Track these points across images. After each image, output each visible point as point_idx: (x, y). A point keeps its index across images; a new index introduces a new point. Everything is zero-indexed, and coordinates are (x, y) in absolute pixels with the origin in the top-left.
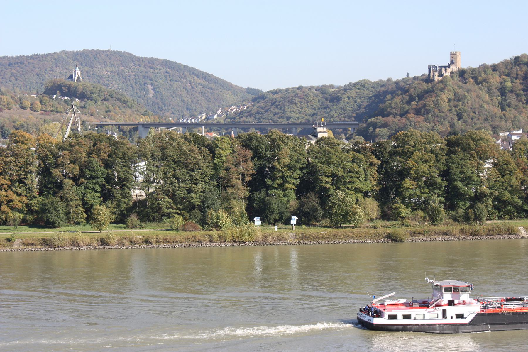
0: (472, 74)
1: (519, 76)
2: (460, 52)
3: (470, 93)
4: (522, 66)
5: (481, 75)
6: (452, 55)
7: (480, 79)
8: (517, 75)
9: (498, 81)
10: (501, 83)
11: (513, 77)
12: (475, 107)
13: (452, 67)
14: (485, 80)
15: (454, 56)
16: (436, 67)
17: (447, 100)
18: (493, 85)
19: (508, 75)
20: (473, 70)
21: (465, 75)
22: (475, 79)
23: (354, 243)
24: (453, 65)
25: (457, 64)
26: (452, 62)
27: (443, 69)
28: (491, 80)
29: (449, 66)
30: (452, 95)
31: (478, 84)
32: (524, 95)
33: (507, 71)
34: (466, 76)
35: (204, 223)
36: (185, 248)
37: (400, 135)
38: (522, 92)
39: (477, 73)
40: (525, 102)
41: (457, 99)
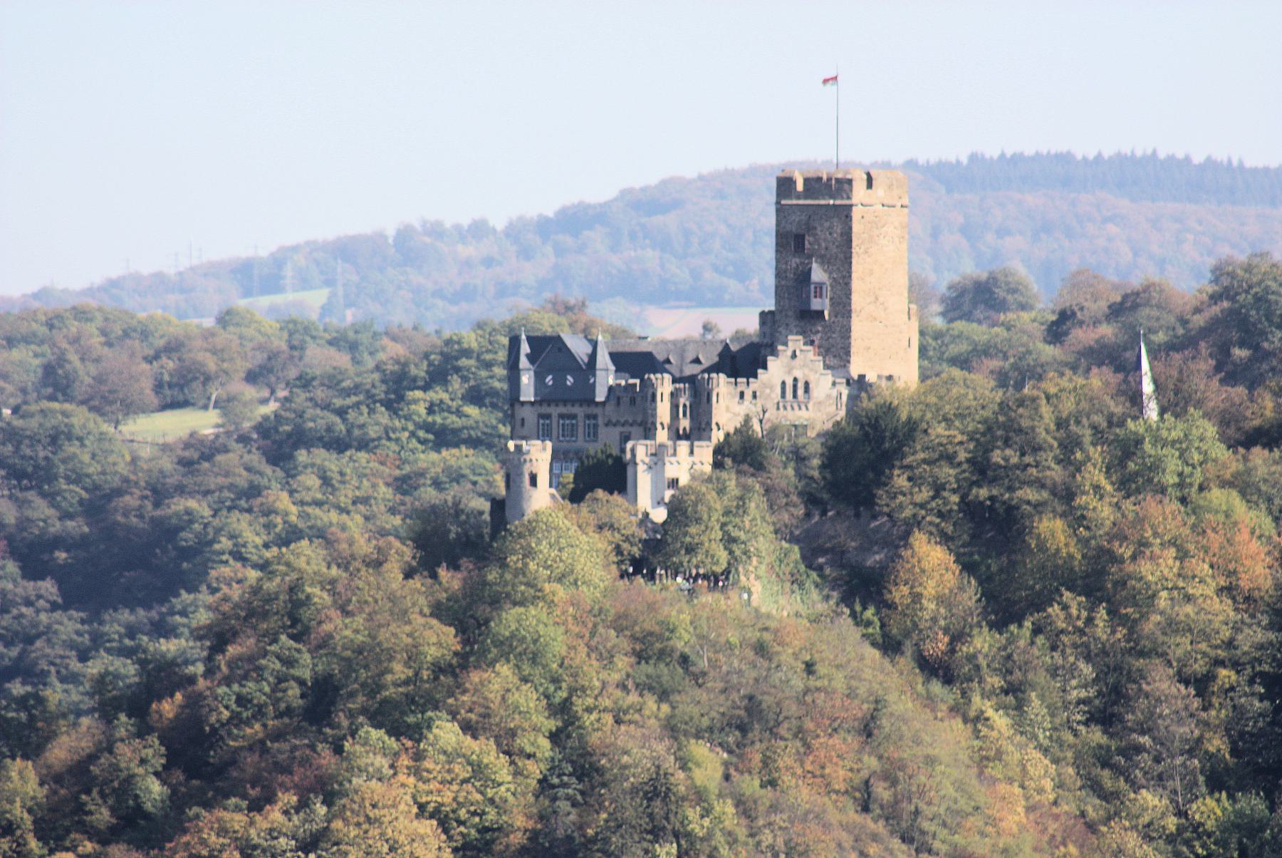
0: (981, 469)
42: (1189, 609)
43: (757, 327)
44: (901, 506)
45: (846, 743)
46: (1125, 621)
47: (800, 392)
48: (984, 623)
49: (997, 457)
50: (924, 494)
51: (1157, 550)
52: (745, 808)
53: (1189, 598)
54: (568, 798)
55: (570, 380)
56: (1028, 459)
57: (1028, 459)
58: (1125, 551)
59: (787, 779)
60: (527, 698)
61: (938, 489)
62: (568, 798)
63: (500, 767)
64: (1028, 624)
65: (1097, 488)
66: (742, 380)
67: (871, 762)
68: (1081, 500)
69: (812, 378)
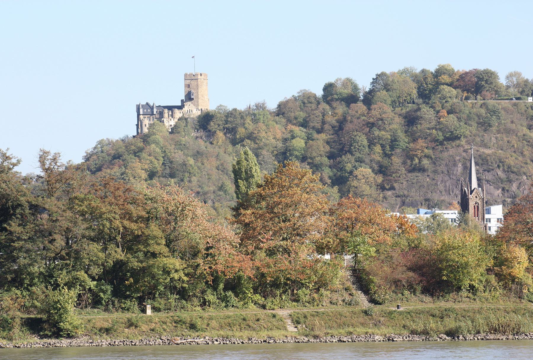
0: (227, 122)
1: (327, 127)
2: (206, 75)
3: (200, 160)
4: (335, 104)
5: (244, 124)
6: (188, 82)
7: (241, 132)
8: (324, 123)
9: (279, 136)
10: (285, 140)
11: (313, 128)
12: (206, 189)
13: (186, 109)
14: (250, 137)
15: (193, 83)
16: (152, 108)
17: (144, 175)
18: (266, 145)
19: (304, 124)
20: (231, 115)
21: (212, 124)
22: (230, 131)
23: (269, 343)
24: (189, 103)
25: (200, 101)
26: (189, 97)
27: (166, 111)
28: (263, 134)
29: (180, 108)
30: (158, 165)
31: (234, 142)
32: (330, 167)
33: (302, 115)
34: (212, 126)
35: (58, 333)
36: (80, 347)
37: (503, 234)
38: (325, 160)
39: (239, 121)
40: (329, 181)
41: (168, 171)
42: (268, 141)
43: (78, 160)
44: (213, 129)
45: (214, 159)
46: (257, 143)
47: (191, 112)
48: (44, 317)
49: (229, 119)
50: (217, 126)
51: (262, 132)
52: (199, 168)
53: (268, 140)
54: (168, 166)
55: (149, 111)
56: (235, 120)
57: (235, 120)
58: (256, 132)
59: (206, 164)
60: (158, 150)
61: (219, 125)
62: (168, 166)
63: (156, 162)
64: (239, 144)
65: (248, 123)
66: (180, 110)
67: (218, 163)
68: (246, 125)
69: (193, 109)
